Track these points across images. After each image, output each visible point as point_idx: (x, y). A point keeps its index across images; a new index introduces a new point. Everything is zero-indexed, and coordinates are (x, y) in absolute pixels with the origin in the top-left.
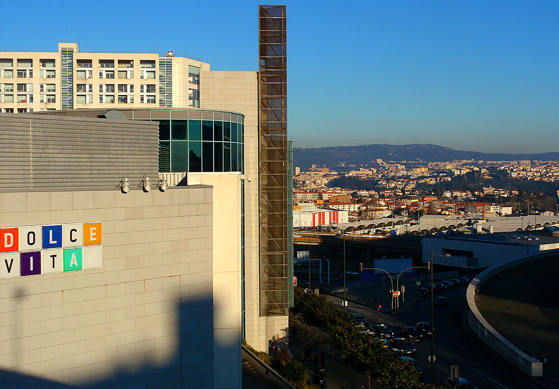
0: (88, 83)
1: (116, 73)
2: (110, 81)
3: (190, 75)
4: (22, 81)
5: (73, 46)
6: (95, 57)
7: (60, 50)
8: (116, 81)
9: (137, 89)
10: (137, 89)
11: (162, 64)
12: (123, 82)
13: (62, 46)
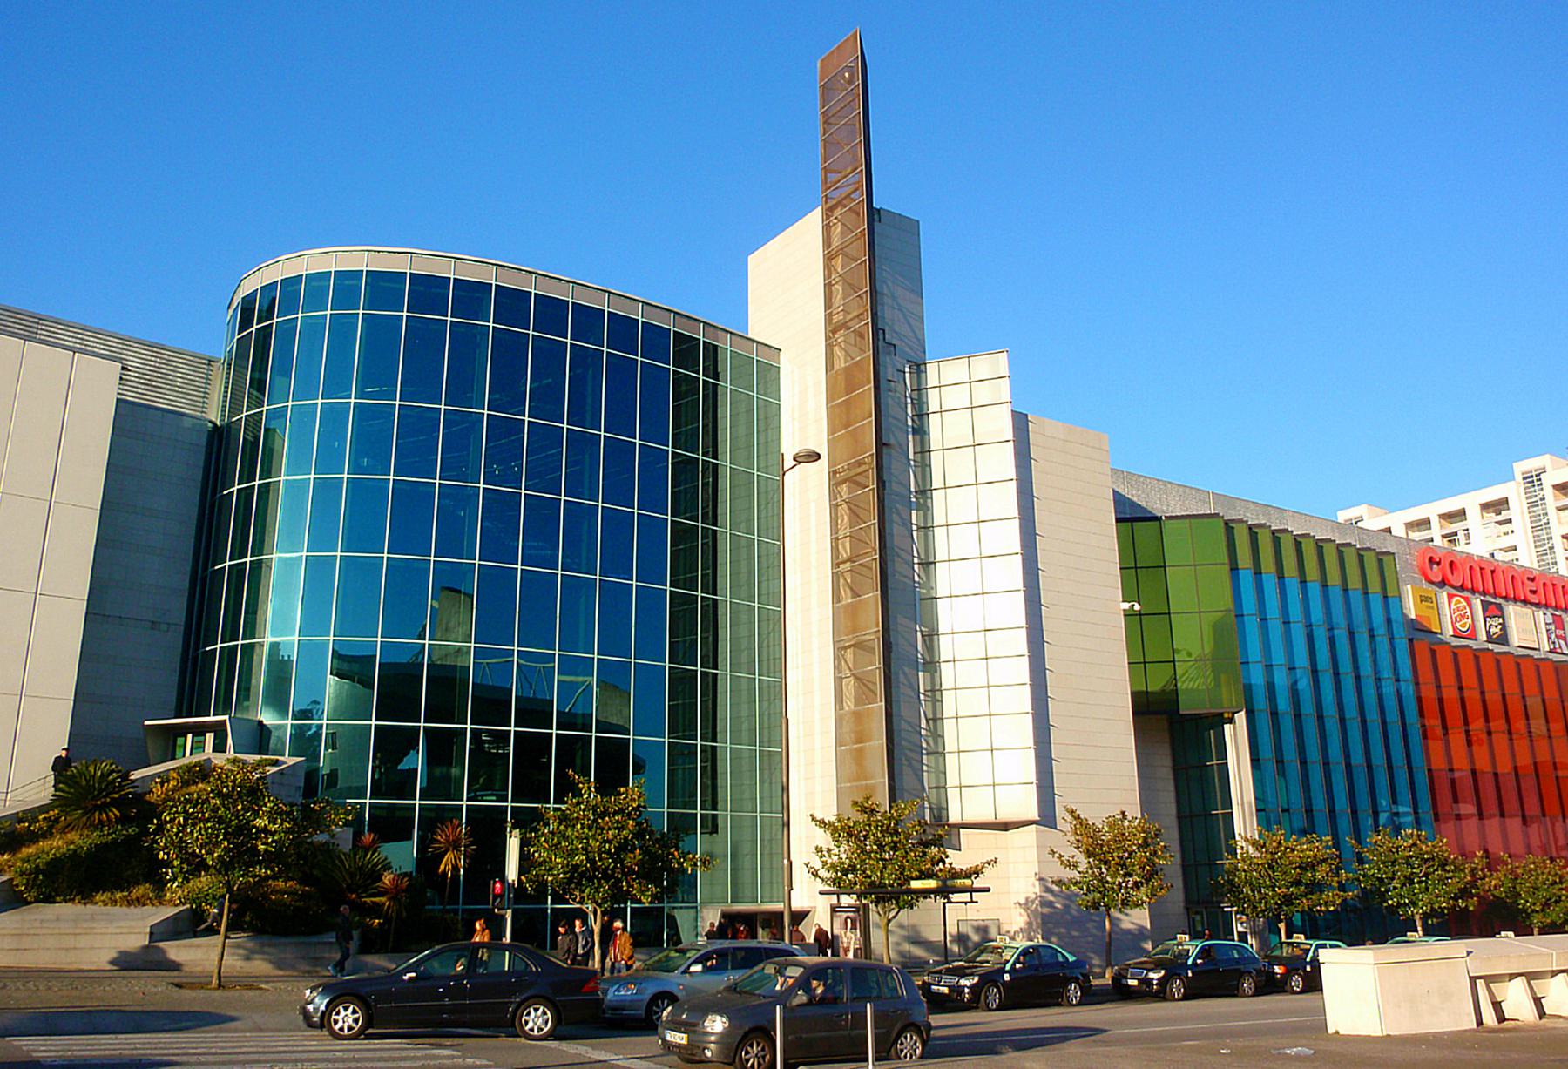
5: (1543, 461)
7: (1519, 477)
13: (1521, 467)
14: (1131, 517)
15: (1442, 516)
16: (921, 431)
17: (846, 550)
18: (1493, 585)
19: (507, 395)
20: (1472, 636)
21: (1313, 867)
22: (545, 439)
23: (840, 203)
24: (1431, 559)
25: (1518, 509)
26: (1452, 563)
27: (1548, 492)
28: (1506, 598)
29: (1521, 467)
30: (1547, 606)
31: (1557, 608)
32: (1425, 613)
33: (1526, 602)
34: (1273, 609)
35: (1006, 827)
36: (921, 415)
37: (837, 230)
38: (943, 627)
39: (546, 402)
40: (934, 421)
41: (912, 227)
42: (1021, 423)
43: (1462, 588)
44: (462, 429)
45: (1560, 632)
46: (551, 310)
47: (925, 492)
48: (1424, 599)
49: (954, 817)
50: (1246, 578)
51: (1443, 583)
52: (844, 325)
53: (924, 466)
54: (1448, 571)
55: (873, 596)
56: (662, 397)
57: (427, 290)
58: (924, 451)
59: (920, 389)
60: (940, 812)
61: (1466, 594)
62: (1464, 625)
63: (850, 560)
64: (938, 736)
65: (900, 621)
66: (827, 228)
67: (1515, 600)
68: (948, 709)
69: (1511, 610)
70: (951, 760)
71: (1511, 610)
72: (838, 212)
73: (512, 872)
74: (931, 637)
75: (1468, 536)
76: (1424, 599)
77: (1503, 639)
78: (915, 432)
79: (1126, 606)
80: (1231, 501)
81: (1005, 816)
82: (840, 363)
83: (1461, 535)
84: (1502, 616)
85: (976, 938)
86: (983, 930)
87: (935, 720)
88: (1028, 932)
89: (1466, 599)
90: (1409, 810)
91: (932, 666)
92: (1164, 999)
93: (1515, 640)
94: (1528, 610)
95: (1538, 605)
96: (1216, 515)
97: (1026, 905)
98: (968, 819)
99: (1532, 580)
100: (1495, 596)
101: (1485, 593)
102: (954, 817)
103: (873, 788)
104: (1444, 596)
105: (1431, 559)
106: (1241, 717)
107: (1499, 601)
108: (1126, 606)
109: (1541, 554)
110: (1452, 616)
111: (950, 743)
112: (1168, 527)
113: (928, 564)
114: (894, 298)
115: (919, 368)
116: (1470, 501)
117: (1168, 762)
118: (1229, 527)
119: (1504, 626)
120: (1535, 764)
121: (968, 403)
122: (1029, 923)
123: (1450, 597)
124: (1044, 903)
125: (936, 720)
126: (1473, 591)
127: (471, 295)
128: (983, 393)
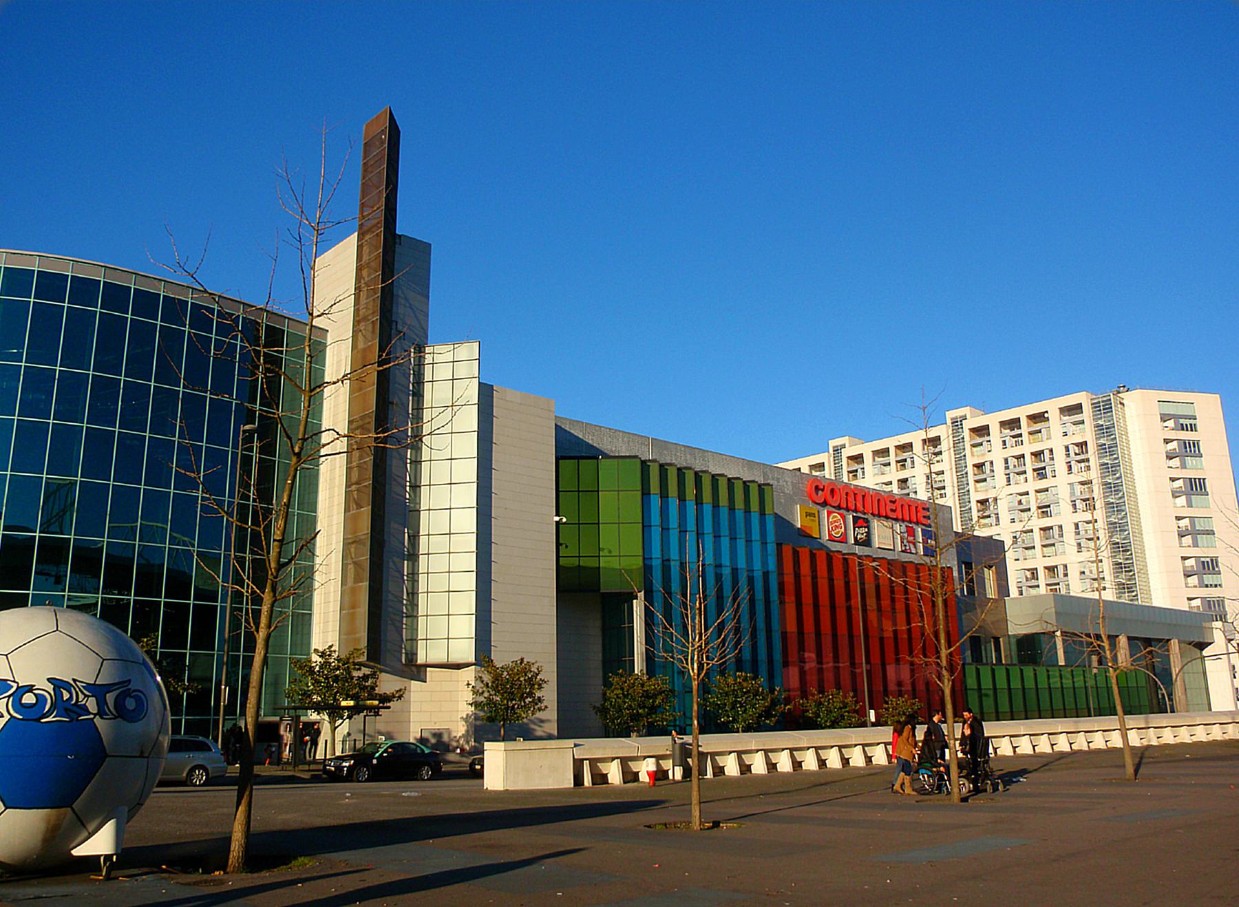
0: (988, 457)
1: (1025, 437)
2: (1018, 451)
3: (1164, 418)
4: (903, 474)
5: (965, 411)
6: (992, 421)
7: (949, 422)
8: (1027, 449)
9: (1060, 455)
10: (1060, 455)
11: (1095, 406)
12: (1037, 447)
13: (950, 415)
14: (573, 453)
15: (897, 447)
16: (418, 395)
17: (355, 475)
18: (865, 506)
19: (108, 361)
20: (843, 539)
21: (654, 697)
22: (136, 393)
23: (369, 231)
24: (817, 488)
25: (945, 445)
26: (832, 490)
27: (966, 434)
29: (950, 415)
30: (903, 520)
31: (910, 522)
32: (809, 522)
33: (887, 517)
34: (674, 522)
35: (458, 666)
36: (419, 382)
37: (366, 249)
38: (423, 530)
39: (139, 366)
40: (427, 386)
41: (424, 249)
42: (486, 393)
43: (839, 507)
44: (72, 385)
45: (911, 539)
46: (146, 302)
47: (418, 437)
48: (808, 514)
49: (421, 659)
50: (655, 501)
51: (825, 504)
52: (365, 319)
53: (418, 418)
54: (827, 495)
55: (367, 510)
56: (255, 360)
57: (51, 284)
58: (419, 408)
59: (420, 365)
60: (412, 655)
62: (837, 533)
63: (357, 483)
64: (414, 604)
65: (392, 526)
66: (360, 248)
67: (879, 516)
68: (422, 587)
69: (876, 524)
70: (421, 621)
71: (876, 524)
72: (367, 237)
73: (639, 666)
74: (415, 537)
76: (808, 514)
77: (867, 542)
78: (414, 395)
79: (557, 519)
81: (456, 658)
82: (361, 345)
84: (868, 527)
85: (433, 741)
86: (438, 735)
87: (413, 594)
88: (466, 736)
90: (813, 655)
91: (414, 557)
92: (351, 781)
93: (876, 542)
95: (896, 520)
96: (636, 457)
97: (466, 719)
98: (430, 661)
99: (894, 502)
101: (856, 511)
102: (421, 659)
103: (359, 640)
105: (817, 488)
106: (641, 595)
108: (557, 519)
110: (830, 527)
111: (422, 610)
112: (604, 463)
113: (416, 487)
114: (406, 299)
115: (420, 349)
116: (867, 449)
117: (598, 623)
118: (644, 464)
119: (868, 533)
121: (451, 376)
122: (467, 731)
123: (829, 513)
124: (476, 719)
125: (413, 594)
126: (848, 509)
127: (85, 289)
128: (462, 370)
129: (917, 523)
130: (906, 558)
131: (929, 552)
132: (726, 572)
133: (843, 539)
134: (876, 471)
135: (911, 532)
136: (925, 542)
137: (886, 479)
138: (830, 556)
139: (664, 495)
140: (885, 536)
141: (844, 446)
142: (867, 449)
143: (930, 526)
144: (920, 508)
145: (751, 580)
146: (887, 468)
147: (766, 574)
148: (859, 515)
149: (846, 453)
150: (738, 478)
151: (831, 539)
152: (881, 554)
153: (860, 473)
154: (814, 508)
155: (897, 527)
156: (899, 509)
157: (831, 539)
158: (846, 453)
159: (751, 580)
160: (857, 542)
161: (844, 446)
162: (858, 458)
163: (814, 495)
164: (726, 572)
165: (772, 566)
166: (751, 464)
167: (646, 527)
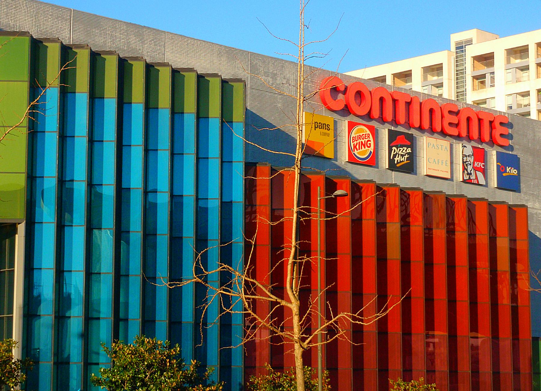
13: (456, 38)
18: (403, 116)
20: (372, 161)
24: (335, 90)
28: (421, 129)
29: (456, 38)
30: (469, 138)
32: (317, 137)
33: (443, 133)
43: (369, 116)
48: (319, 126)
50: (52, 95)
51: (347, 111)
61: (373, 123)
62: (362, 153)
67: (432, 131)
75: (493, 79)
76: (319, 126)
77: (410, 167)
80: (92, 21)
83: (488, 76)
89: (372, 129)
94: (444, 143)
95: (459, 137)
99: (457, 113)
100: (409, 125)
101: (395, 122)
104: (344, 124)
107: (412, 131)
109: (449, 95)
110: (348, 144)
116: (499, 47)
118: (37, 47)
120: (102, 185)
123: (351, 126)
126: (382, 120)
129: (493, 142)
130: (471, 192)
131: (509, 184)
132: (163, 200)
133: (372, 161)
134: (510, 77)
135: (480, 155)
136: (500, 171)
137: (522, 88)
138: (356, 188)
139: (201, 116)
140: (438, 161)
141: (469, 42)
142: (499, 47)
143: (511, 148)
144: (497, 124)
145: (201, 214)
146: (525, 74)
147: (226, 207)
148: (400, 129)
149: (472, 51)
150: (215, 75)
151: (353, 160)
152: (430, 186)
153: (488, 79)
154: (329, 118)
155: (458, 147)
156: (464, 124)
157: (353, 160)
158: (472, 51)
159: (201, 214)
160: (392, 166)
161: (469, 42)
162: (487, 59)
163: (328, 99)
164: (163, 200)
165: (238, 194)
166: (232, 53)
167: (34, 133)
